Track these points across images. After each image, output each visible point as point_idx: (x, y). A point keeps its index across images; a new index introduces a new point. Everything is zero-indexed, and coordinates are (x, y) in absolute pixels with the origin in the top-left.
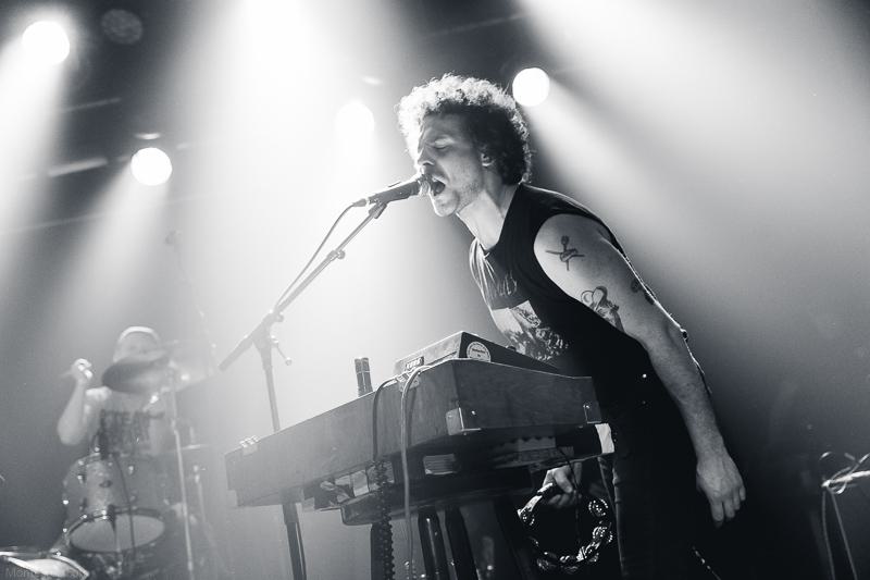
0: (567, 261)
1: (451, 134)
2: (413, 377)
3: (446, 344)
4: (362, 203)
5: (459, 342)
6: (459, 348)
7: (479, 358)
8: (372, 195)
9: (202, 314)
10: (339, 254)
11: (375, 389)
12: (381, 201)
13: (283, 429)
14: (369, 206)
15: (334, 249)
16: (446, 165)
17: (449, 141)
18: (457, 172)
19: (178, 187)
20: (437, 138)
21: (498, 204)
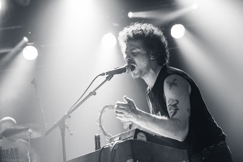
0: (171, 86)
1: (139, 48)
2: (116, 144)
3: (129, 132)
4: (103, 74)
5: (134, 132)
6: (134, 135)
7: (142, 139)
8: (107, 71)
9: (43, 112)
10: (94, 93)
11: (101, 148)
12: (110, 75)
13: (67, 161)
14: (106, 76)
15: (92, 91)
16: (136, 60)
17: (138, 50)
18: (141, 63)
19: (39, 62)
20: (133, 49)
21: (156, 73)
